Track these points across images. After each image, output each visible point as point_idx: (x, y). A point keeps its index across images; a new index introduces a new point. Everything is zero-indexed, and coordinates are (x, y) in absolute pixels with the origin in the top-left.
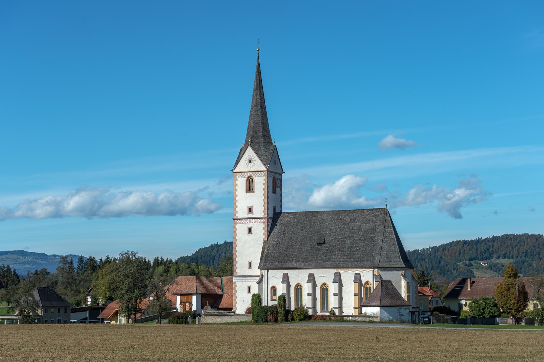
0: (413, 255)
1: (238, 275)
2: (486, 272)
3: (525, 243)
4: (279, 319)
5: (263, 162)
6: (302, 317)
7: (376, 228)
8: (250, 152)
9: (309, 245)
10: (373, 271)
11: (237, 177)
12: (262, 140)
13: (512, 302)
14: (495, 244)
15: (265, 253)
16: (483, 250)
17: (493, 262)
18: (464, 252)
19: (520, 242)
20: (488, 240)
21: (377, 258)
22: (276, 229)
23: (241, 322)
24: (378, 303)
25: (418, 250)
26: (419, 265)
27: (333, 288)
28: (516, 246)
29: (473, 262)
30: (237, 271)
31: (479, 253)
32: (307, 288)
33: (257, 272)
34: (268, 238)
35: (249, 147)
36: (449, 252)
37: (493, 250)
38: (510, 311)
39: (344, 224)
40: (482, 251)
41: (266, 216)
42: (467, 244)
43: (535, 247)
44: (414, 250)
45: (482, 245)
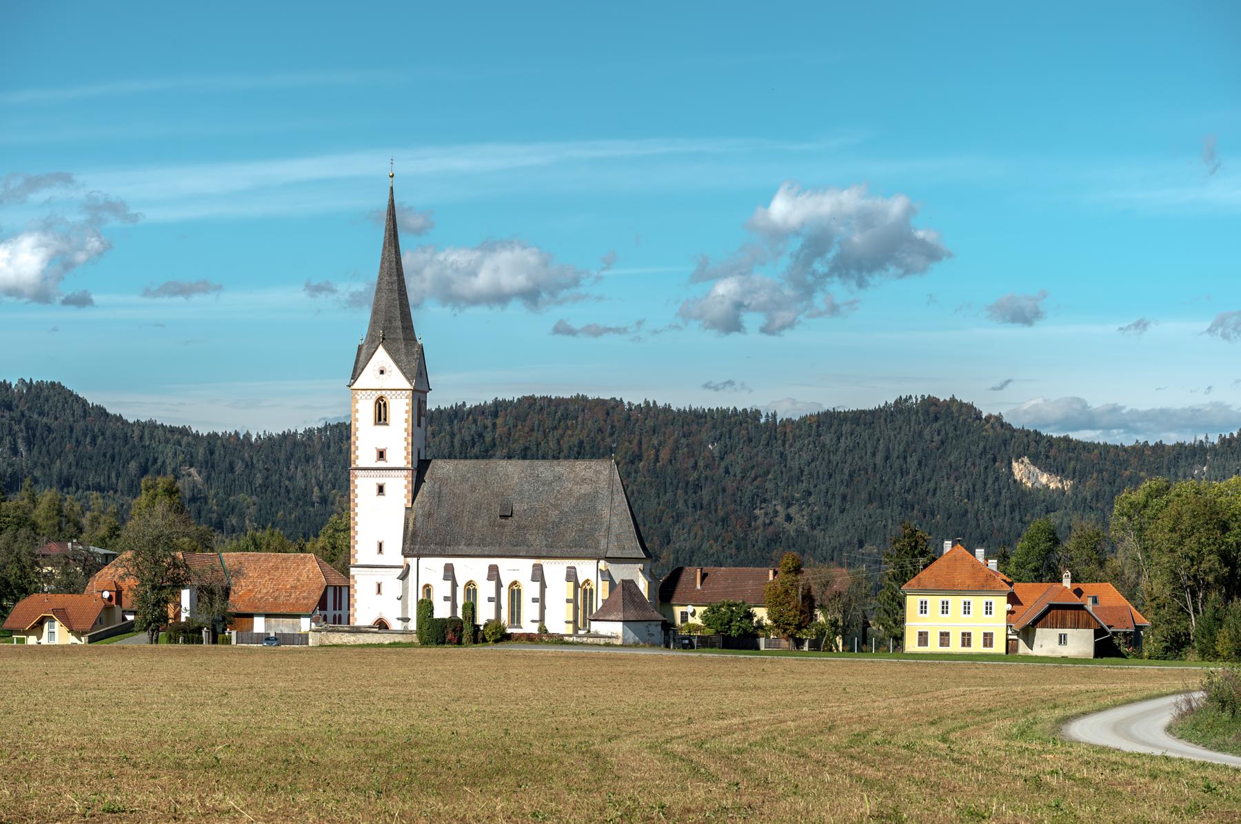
0: (281, 446)
1: (359, 563)
3: (577, 422)
4: (464, 640)
5: (404, 374)
6: (499, 636)
7: (597, 492)
8: (381, 357)
9: (486, 518)
10: (598, 562)
11: (358, 397)
12: (401, 336)
14: (499, 421)
15: (410, 529)
16: (468, 438)
19: (565, 417)
20: (480, 410)
21: (603, 542)
22: (425, 487)
24: (621, 616)
25: (296, 433)
26: (299, 474)
27: (530, 590)
28: (555, 428)
30: (357, 556)
32: (486, 589)
33: (400, 561)
34: (413, 503)
35: (381, 348)
37: (494, 439)
38: (788, 627)
39: (544, 484)
40: (466, 439)
41: (410, 466)
43: (602, 432)
44: (284, 432)
45: (466, 425)
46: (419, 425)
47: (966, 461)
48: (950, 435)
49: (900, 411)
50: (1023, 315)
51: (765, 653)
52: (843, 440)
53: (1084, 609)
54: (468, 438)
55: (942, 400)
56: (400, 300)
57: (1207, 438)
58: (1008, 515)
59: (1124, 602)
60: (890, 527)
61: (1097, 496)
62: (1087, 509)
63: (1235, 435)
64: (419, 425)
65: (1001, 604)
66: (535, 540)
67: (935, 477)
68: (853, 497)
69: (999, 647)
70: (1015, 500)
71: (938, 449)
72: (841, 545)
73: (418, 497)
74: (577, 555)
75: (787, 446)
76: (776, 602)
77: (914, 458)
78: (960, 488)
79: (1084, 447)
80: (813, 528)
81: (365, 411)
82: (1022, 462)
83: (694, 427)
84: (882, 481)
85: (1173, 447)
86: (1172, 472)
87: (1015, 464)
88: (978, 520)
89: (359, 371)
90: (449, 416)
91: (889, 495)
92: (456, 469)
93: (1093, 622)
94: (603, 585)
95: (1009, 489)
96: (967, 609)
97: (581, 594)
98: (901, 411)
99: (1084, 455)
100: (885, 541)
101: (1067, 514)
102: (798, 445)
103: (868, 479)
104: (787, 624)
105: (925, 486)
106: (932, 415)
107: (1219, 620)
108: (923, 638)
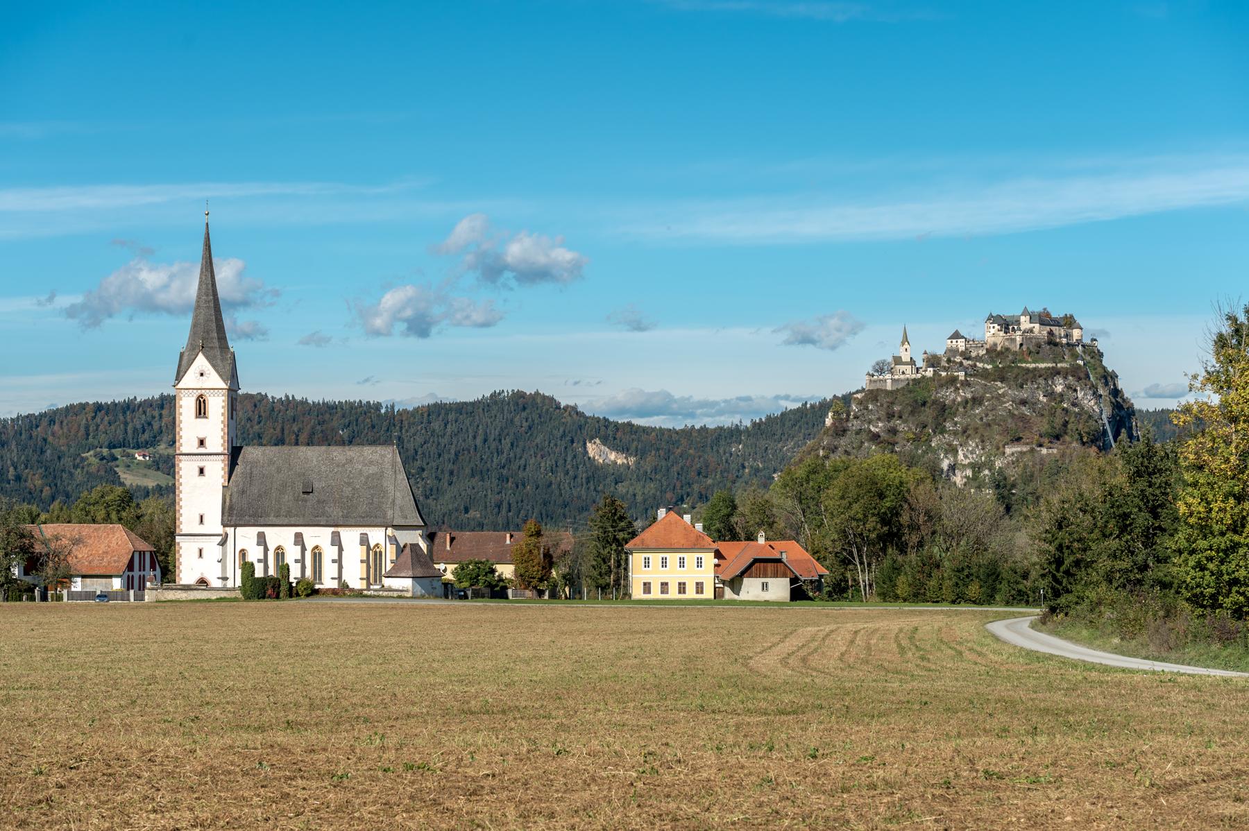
1: (183, 532)
2: (146, 475)
4: (281, 595)
5: (221, 376)
8: (201, 362)
12: (217, 344)
13: (536, 568)
15: (227, 504)
16: (139, 426)
17: (161, 452)
18: (97, 430)
21: (390, 513)
22: (238, 469)
23: (221, 599)
24: (410, 574)
27: (329, 553)
29: (117, 452)
30: (181, 527)
31: (130, 431)
32: (292, 554)
33: (220, 529)
34: (229, 482)
36: (62, 428)
39: (338, 466)
41: (226, 452)
42: (103, 412)
46: (232, 418)
47: (550, 442)
48: (536, 422)
49: (494, 403)
50: (639, 327)
51: (512, 602)
52: (449, 426)
53: (782, 562)
54: (139, 426)
55: (528, 393)
56: (216, 315)
57: (741, 422)
58: (584, 486)
59: (808, 556)
60: (489, 496)
61: (655, 470)
62: (648, 480)
63: (763, 420)
64: (232, 418)
65: (709, 559)
66: (333, 512)
67: (525, 456)
68: (458, 472)
69: (708, 594)
70: (590, 474)
71: (526, 433)
72: (450, 511)
73: (233, 477)
74: (369, 523)
75: (403, 431)
76: (521, 560)
77: (508, 440)
78: (546, 464)
79: (644, 430)
80: (427, 497)
81: (186, 406)
82: (595, 443)
83: (327, 416)
84: (482, 459)
85: (715, 429)
86: (715, 450)
87: (589, 445)
88: (560, 490)
89: (182, 374)
90: (123, 408)
91: (488, 470)
92: (263, 454)
93: (788, 572)
94: (391, 548)
95: (585, 464)
96: (682, 563)
97: (373, 557)
98: (496, 403)
99: (644, 437)
100: (486, 507)
101: (632, 485)
102: (412, 430)
103: (470, 458)
104: (531, 578)
105: (517, 463)
106: (521, 406)
107: (896, 569)
108: (647, 587)
